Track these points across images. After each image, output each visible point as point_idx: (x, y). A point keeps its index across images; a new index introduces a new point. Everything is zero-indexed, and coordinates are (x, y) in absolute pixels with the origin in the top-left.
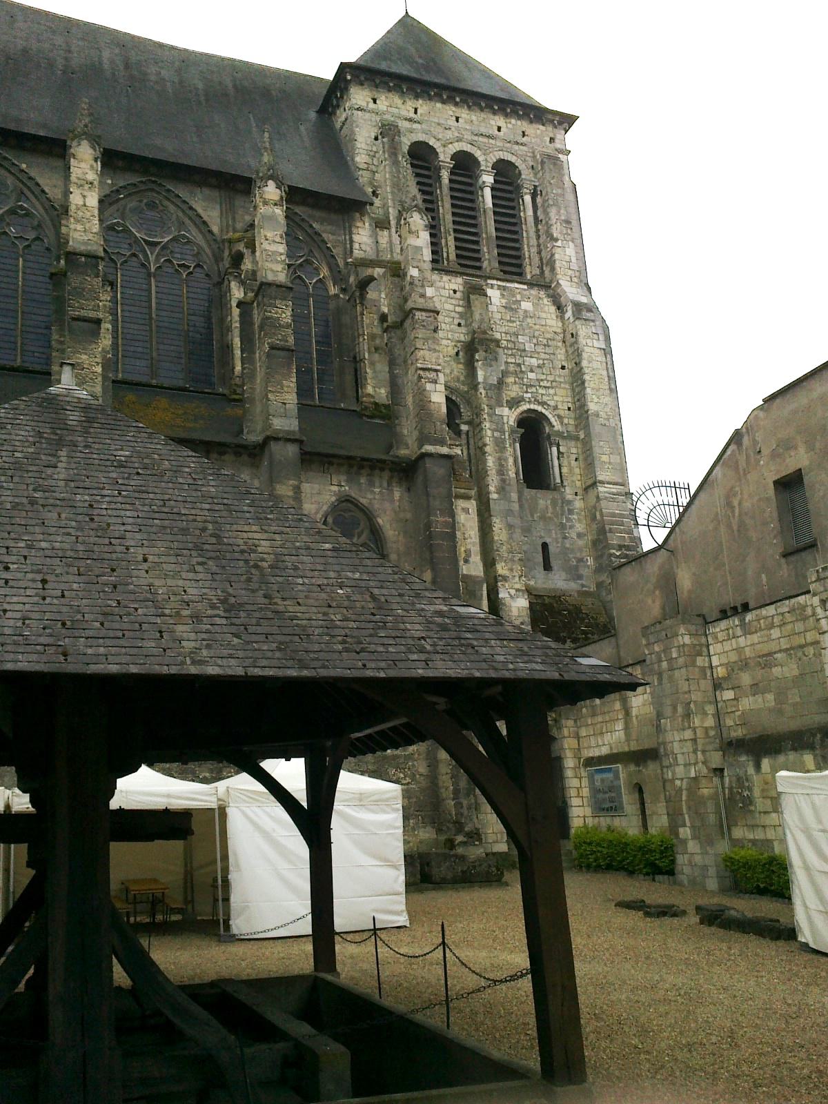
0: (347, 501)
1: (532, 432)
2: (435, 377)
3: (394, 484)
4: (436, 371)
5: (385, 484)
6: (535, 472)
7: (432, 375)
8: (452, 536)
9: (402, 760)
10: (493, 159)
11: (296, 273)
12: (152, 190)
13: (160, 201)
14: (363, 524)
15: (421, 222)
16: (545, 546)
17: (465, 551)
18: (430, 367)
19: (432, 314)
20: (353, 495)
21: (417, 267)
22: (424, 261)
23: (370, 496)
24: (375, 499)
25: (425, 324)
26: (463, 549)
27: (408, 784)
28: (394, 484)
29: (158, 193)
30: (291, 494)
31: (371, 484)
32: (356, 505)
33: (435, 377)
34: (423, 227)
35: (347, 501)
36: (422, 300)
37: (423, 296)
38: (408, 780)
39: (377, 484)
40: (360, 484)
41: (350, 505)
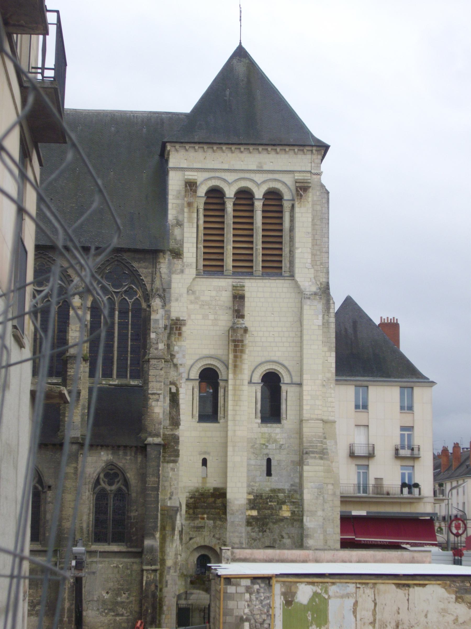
0: (112, 465)
1: (272, 383)
2: (158, 398)
3: (138, 454)
4: (159, 394)
5: (133, 454)
6: (272, 410)
7: (156, 397)
8: (157, 489)
9: (125, 604)
10: (264, 189)
11: (122, 296)
12: (41, 257)
13: (46, 263)
14: (120, 476)
15: (160, 303)
16: (269, 461)
17: (170, 493)
18: (155, 392)
19: (160, 360)
20: (115, 461)
21: (155, 332)
22: (159, 328)
23: (124, 461)
24: (126, 463)
25: (155, 366)
26: (169, 491)
27: (128, 616)
28: (138, 454)
29: (44, 259)
30: (72, 471)
31: (125, 454)
32: (116, 467)
33: (158, 398)
34: (161, 307)
35: (112, 465)
36: (156, 351)
37: (157, 349)
38: (128, 614)
39: (129, 454)
40: (119, 455)
41: (113, 466)
